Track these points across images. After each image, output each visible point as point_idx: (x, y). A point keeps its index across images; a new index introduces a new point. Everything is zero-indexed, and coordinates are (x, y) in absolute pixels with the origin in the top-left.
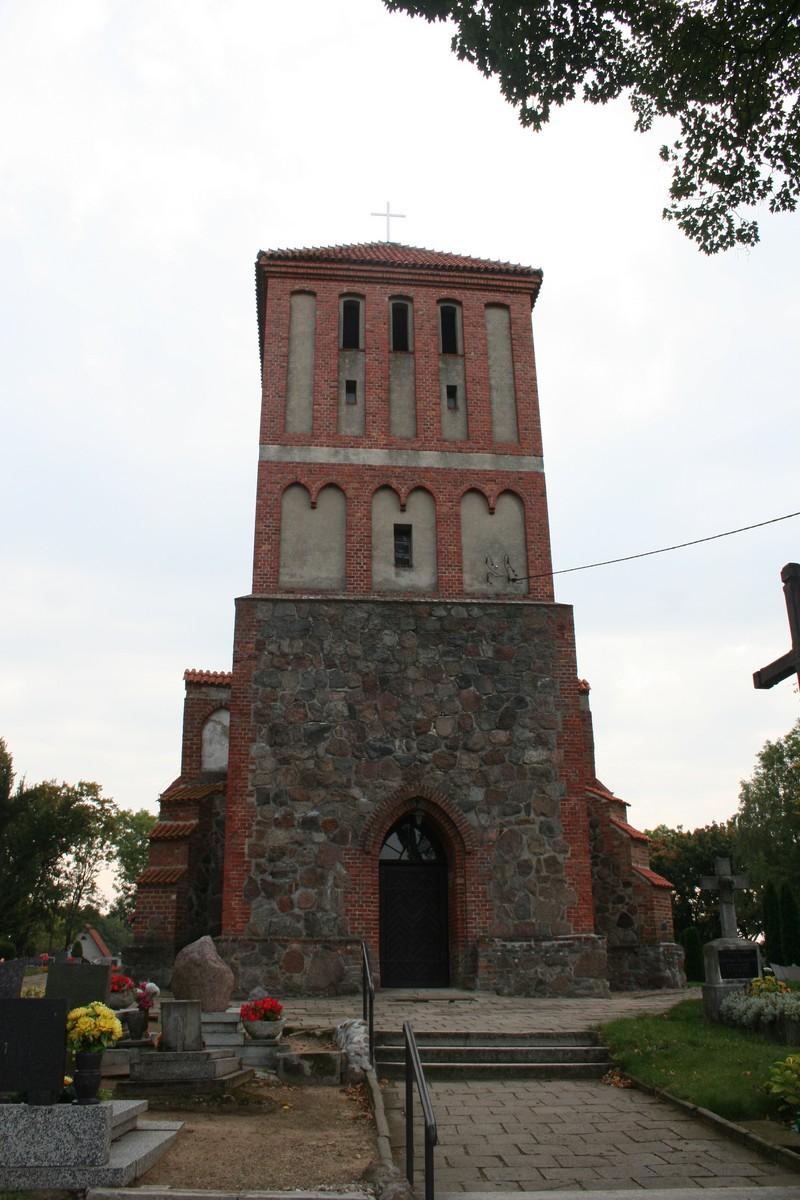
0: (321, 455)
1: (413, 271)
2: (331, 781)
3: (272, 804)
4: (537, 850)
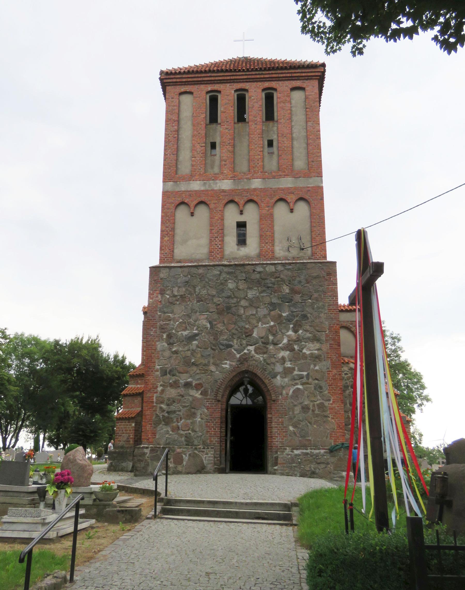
0: (196, 186)
1: (247, 73)
2: (199, 363)
3: (168, 375)
4: (312, 399)
